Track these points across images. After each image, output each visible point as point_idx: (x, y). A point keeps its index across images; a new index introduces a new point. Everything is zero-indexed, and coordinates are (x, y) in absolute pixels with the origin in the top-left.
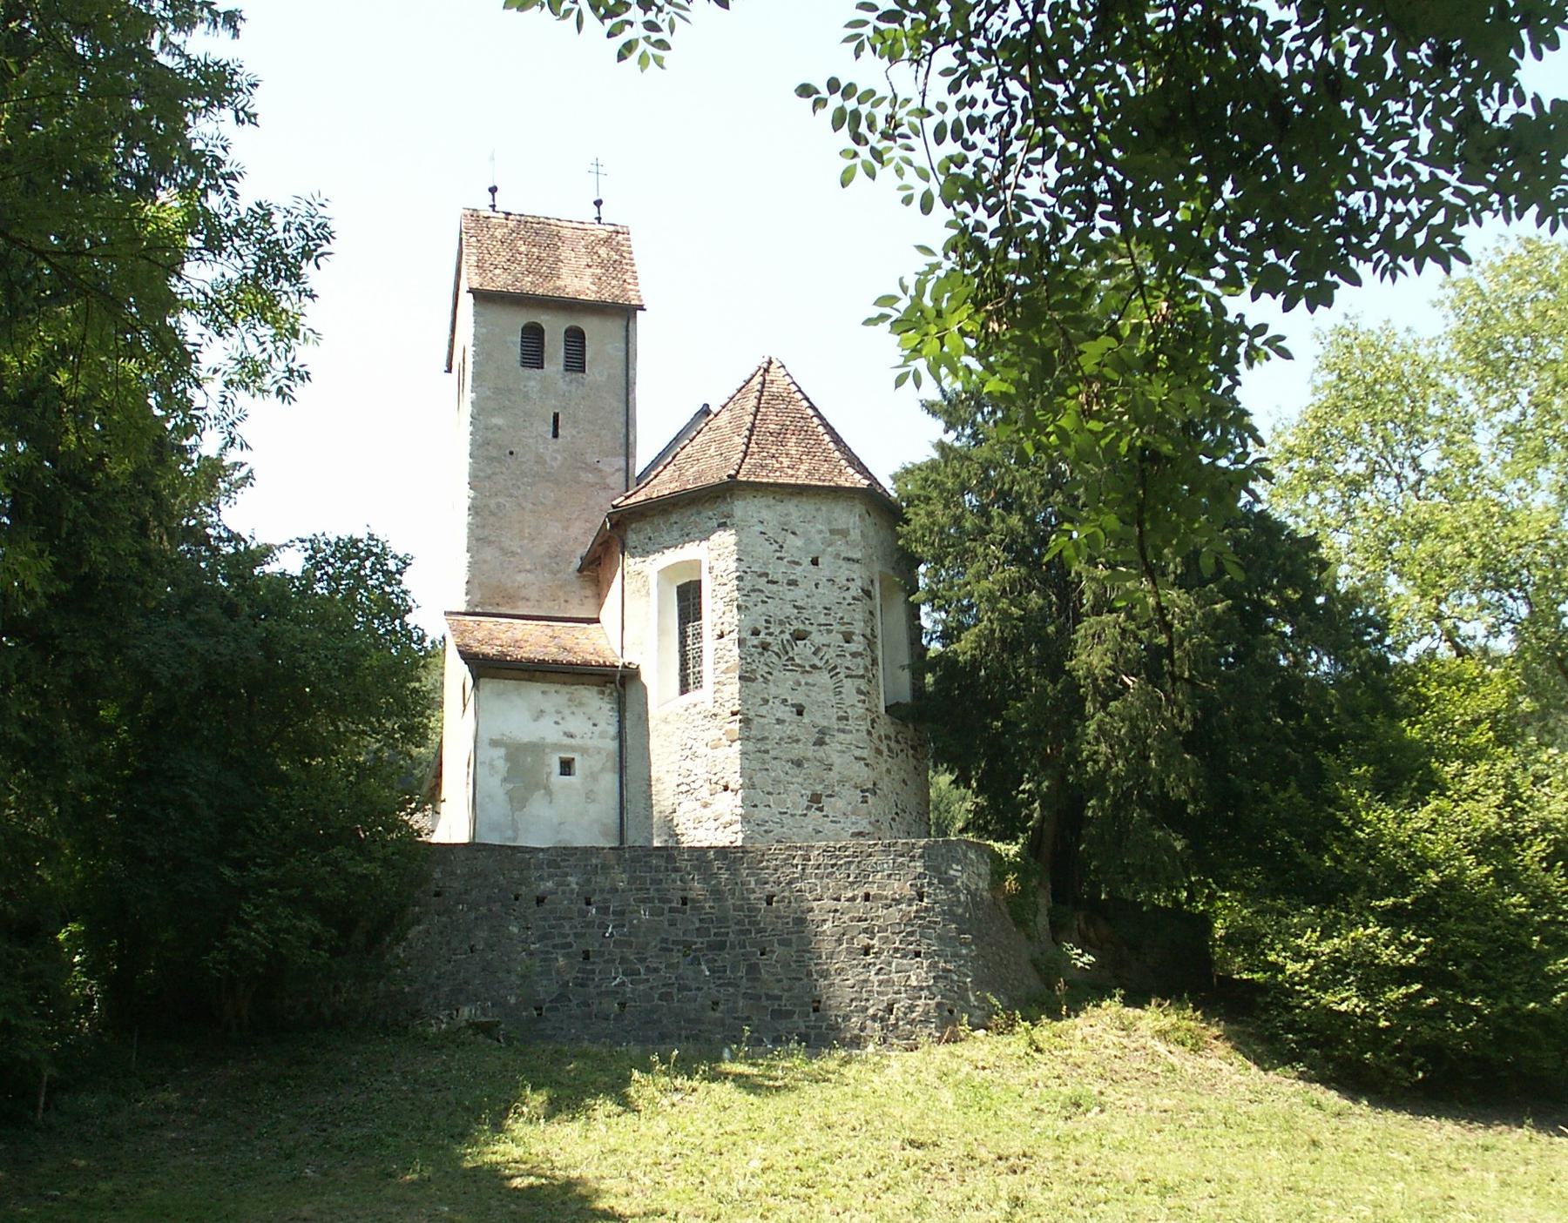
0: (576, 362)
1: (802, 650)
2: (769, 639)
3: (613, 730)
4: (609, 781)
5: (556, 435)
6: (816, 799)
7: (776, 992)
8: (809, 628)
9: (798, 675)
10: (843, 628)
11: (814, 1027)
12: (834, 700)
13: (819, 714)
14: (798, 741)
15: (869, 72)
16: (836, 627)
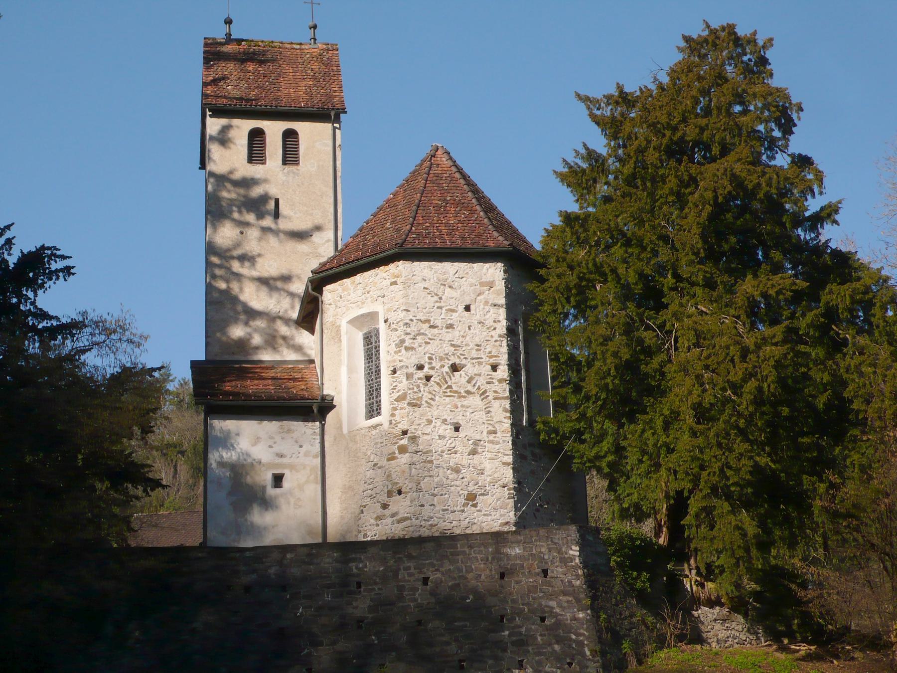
2: (431, 372)
9: (456, 400)
10: (492, 361)
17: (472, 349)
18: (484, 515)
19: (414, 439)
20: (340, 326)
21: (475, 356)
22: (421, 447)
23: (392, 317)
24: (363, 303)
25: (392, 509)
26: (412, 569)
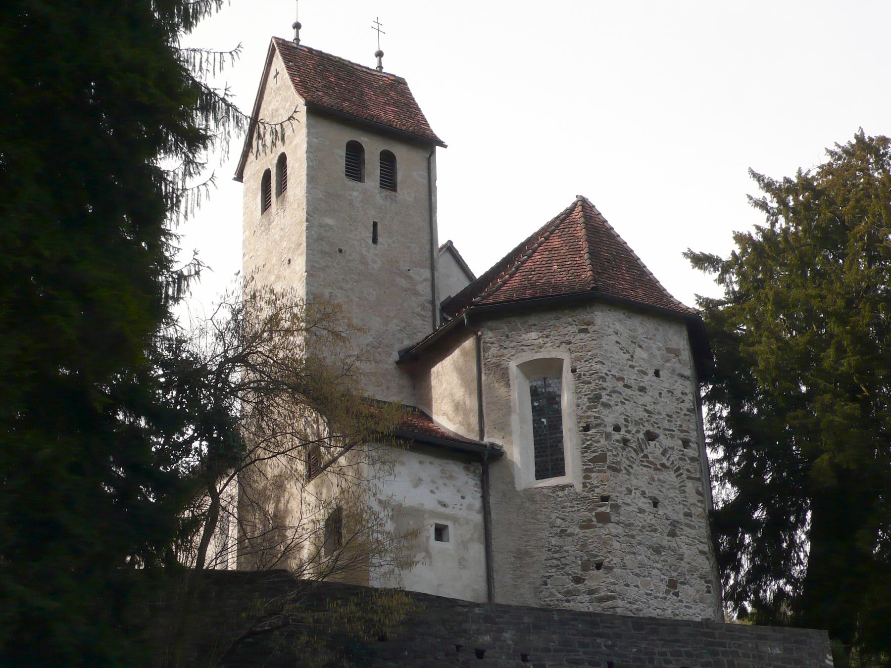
0: (389, 181)
2: (629, 436)
3: (478, 504)
4: (477, 551)
5: (375, 241)
8: (657, 431)
9: (652, 471)
10: (682, 435)
12: (680, 498)
13: (670, 508)
14: (655, 531)
16: (677, 433)
17: (664, 418)
18: (686, 607)
19: (616, 507)
20: (507, 368)
21: (667, 427)
22: (622, 518)
23: (582, 368)
24: (541, 347)
25: (591, 584)
26: (669, 654)
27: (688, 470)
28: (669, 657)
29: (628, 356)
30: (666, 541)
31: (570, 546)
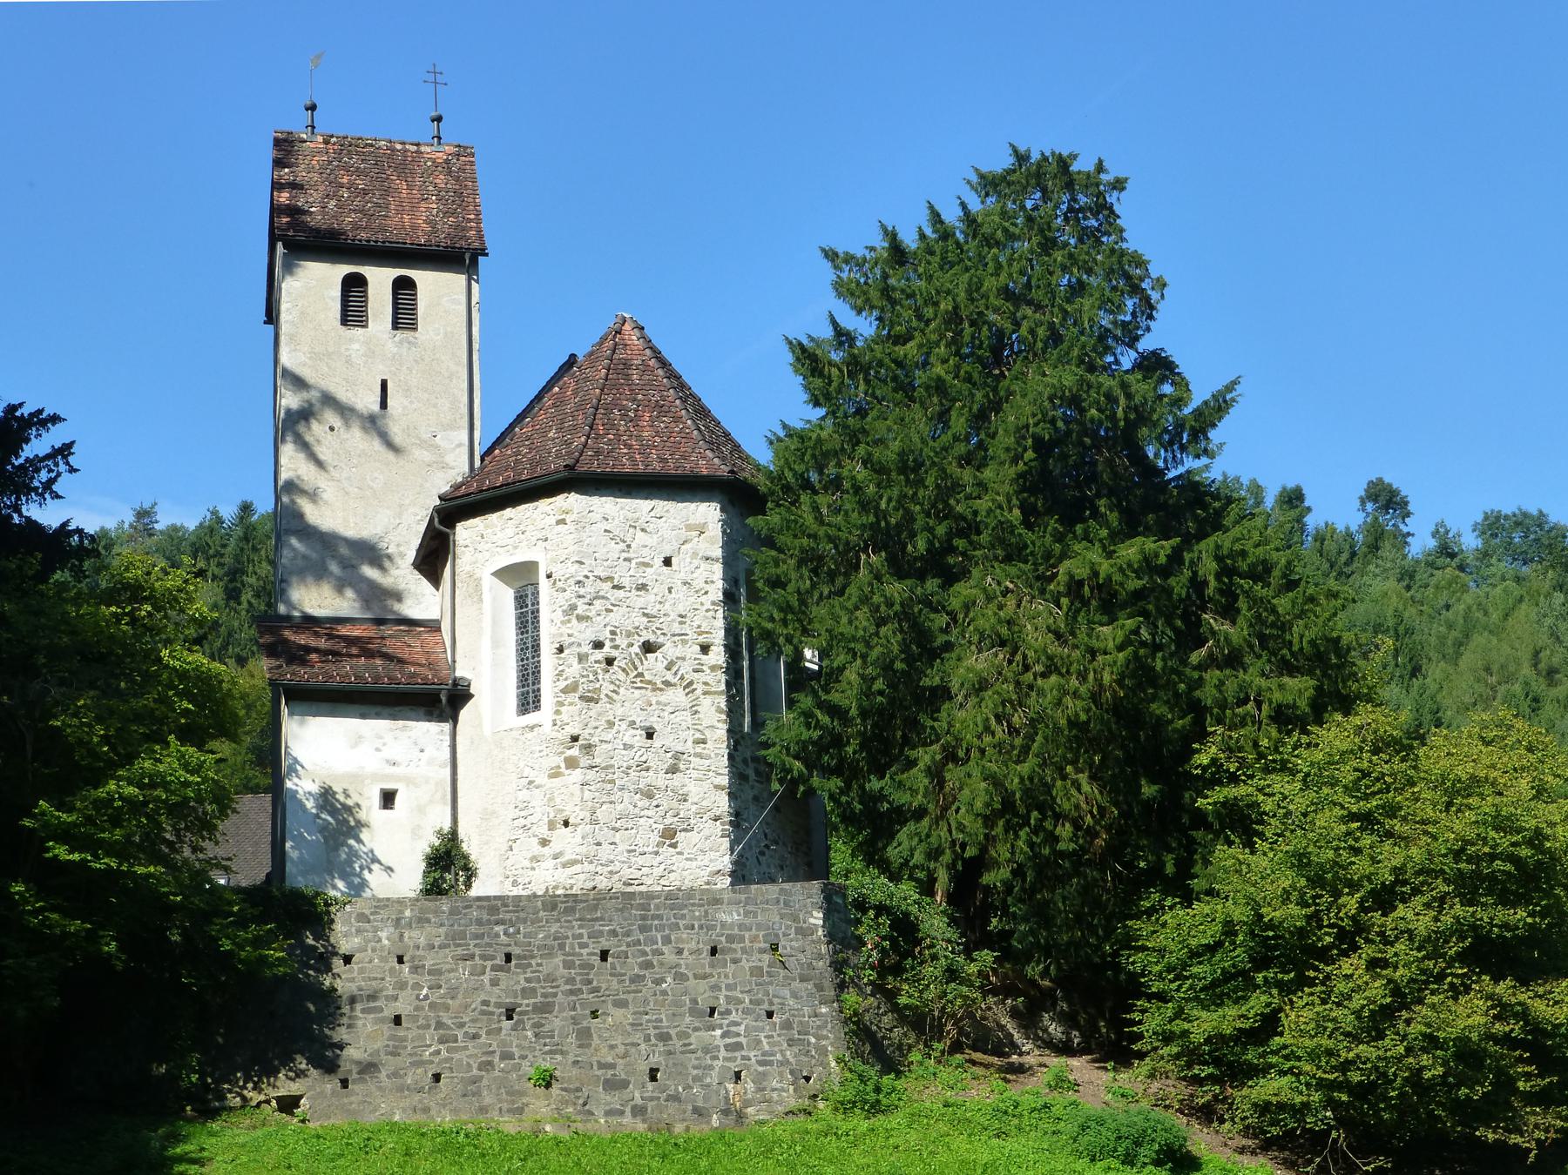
1: (655, 663)
2: (615, 653)
6: (669, 834)
7: (610, 1059)
8: (661, 639)
9: (649, 693)
10: (701, 639)
11: (652, 1099)
15: (1186, 1026)
19: (588, 748)
22: (597, 761)
25: (555, 847)
27: (706, 684)
28: (585, 939)
29: (622, 546)
30: (660, 780)
31: (537, 799)
